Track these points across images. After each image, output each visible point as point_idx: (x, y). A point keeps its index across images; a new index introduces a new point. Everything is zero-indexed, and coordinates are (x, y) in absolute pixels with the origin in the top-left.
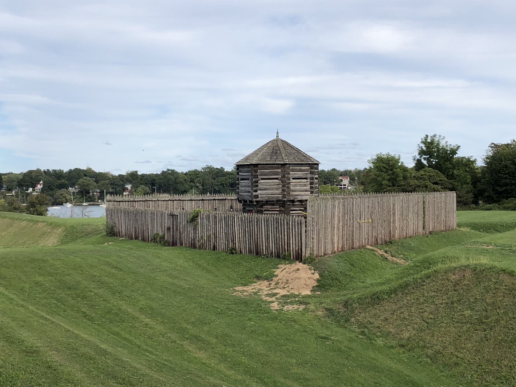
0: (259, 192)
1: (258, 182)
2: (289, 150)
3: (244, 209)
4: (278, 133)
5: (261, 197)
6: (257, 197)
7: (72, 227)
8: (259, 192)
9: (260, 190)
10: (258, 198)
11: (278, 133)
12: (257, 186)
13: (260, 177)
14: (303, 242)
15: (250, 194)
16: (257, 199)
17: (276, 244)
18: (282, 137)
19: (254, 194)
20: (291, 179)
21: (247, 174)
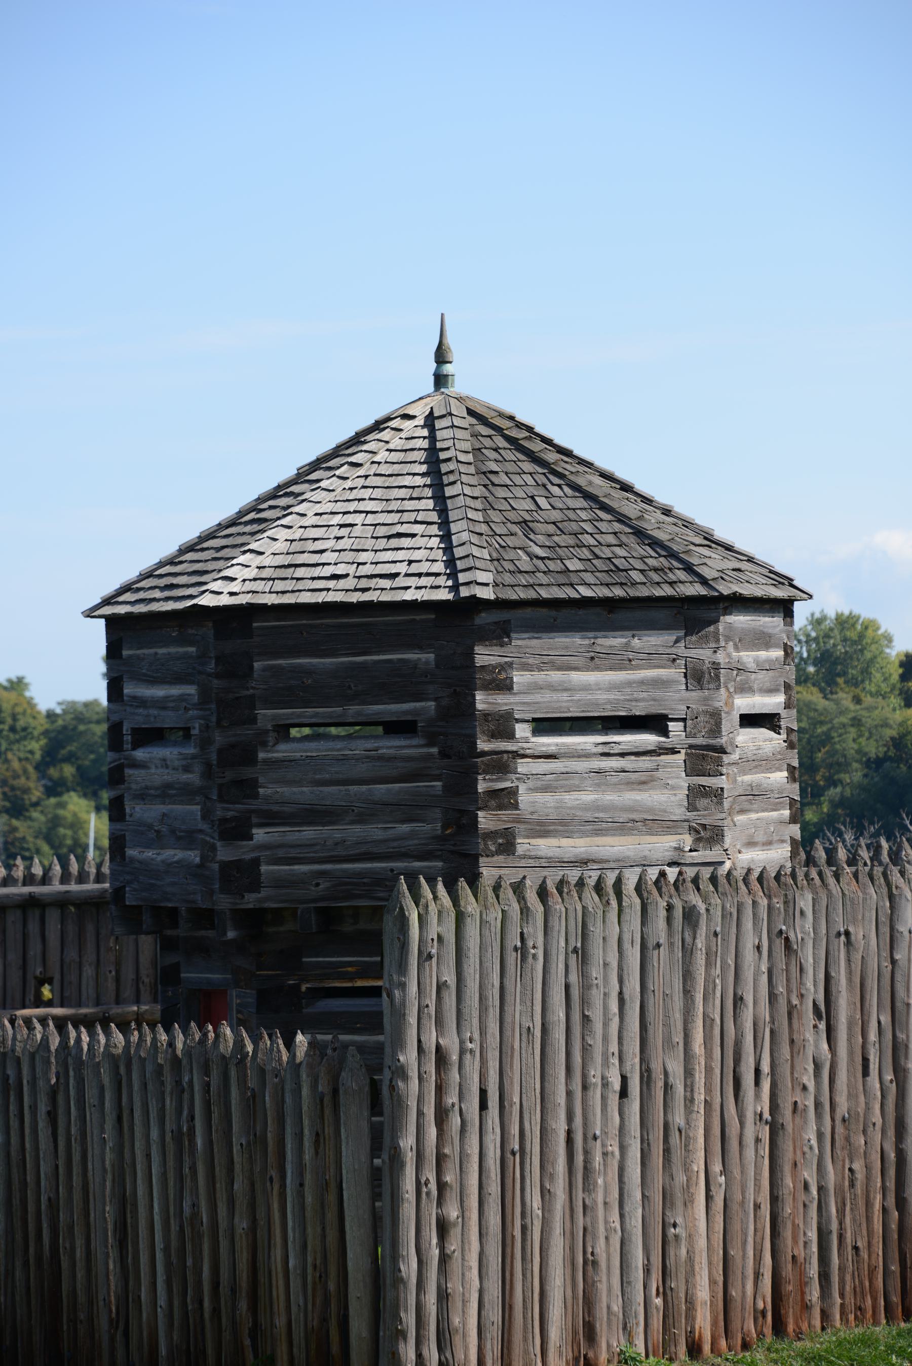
0: (260, 834)
1: (251, 760)
2: (522, 487)
3: (168, 976)
4: (441, 356)
5: (280, 883)
6: (242, 875)
7: (404, 1015)
8: (260, 834)
9: (271, 819)
10: (255, 885)
11: (441, 356)
12: (248, 788)
13: (266, 715)
14: (551, 1018)
15: (194, 856)
16: (250, 900)
17: (771, 691)
18: (472, 381)
19: (225, 853)
20: (522, 730)
21: (175, 691)
